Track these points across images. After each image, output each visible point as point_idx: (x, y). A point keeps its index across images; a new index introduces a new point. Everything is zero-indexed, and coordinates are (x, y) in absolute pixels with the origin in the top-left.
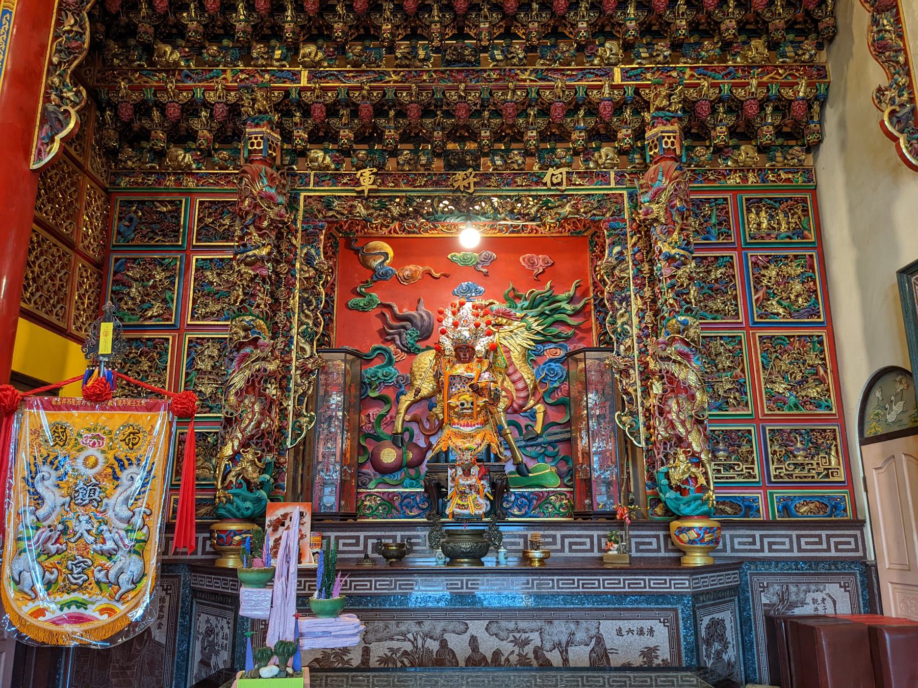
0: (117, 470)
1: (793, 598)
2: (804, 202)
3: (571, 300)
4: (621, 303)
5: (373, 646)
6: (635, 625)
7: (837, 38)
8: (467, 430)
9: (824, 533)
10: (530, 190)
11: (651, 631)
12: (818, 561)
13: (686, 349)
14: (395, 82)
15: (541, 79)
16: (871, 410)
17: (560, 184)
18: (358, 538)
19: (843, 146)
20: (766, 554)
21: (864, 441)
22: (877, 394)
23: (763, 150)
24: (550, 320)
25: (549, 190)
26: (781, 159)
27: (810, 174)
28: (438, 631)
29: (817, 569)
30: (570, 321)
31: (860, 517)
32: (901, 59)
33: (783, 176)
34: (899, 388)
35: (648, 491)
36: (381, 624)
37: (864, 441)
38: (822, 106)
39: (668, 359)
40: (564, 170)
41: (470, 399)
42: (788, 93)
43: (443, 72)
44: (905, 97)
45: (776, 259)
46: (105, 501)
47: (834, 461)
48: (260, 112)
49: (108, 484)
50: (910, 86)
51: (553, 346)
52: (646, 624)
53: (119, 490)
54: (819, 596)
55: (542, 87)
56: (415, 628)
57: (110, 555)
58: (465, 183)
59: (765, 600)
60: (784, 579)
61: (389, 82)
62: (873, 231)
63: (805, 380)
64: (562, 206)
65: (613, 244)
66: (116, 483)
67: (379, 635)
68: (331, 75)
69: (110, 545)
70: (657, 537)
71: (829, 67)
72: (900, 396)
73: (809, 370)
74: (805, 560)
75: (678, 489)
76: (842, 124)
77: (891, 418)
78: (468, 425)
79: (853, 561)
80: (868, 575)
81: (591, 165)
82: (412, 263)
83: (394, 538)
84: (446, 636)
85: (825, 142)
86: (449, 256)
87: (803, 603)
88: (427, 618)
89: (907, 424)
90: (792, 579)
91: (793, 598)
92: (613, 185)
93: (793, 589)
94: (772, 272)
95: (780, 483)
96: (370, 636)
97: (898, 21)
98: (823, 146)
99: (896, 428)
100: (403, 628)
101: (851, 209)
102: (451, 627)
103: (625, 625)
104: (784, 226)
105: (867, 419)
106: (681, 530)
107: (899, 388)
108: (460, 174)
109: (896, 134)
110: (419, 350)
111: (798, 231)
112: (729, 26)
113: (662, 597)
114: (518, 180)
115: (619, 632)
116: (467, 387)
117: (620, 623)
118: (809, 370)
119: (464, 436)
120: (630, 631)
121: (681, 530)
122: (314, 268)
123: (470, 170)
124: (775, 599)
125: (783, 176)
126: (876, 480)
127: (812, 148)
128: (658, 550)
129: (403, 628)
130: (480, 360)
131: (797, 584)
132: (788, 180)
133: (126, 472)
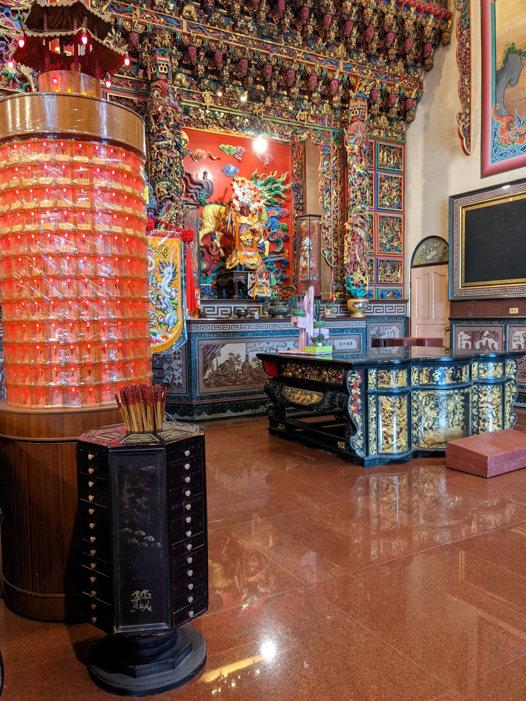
0: (161, 268)
1: (381, 332)
2: (399, 151)
3: (284, 183)
4: (326, 193)
5: (249, 354)
6: (346, 341)
7: (432, 71)
8: (250, 254)
9: (394, 305)
10: (289, 121)
11: (351, 343)
12: (390, 317)
13: (363, 221)
14: (234, 42)
15: (308, 59)
16: (418, 253)
17: (304, 121)
18: (214, 308)
19: (426, 128)
20: (375, 314)
21: (413, 267)
22: (423, 246)
23: (390, 119)
24: (273, 193)
25: (298, 123)
26: (395, 126)
27: (404, 135)
28: (275, 346)
29: (391, 319)
30: (283, 196)
31: (405, 299)
32: (468, 100)
33: (394, 135)
34: (436, 245)
35: (334, 287)
36: (253, 344)
37: (413, 267)
38: (417, 103)
39: (357, 226)
40: (306, 113)
41: (251, 237)
42: (407, 94)
43: (260, 42)
44: (467, 120)
45: (388, 178)
46: (159, 284)
47: (399, 274)
48: (165, 46)
49: (159, 276)
50: (469, 114)
51: (274, 209)
52: (350, 341)
53: (165, 279)
54: (389, 331)
55: (307, 64)
56: (266, 345)
57: (163, 310)
58: (259, 111)
59: (372, 333)
60: (379, 324)
61: (231, 41)
62: (435, 175)
63: (393, 238)
64: (302, 134)
65: (325, 159)
66: (161, 275)
67: (252, 349)
68: (200, 28)
69: (164, 306)
70: (337, 307)
71: (424, 84)
72: (436, 248)
73: (395, 234)
74: (386, 316)
75: (356, 285)
76: (427, 116)
77: (429, 257)
78: (250, 251)
79: (402, 317)
80: (407, 321)
81: (317, 112)
82: (203, 149)
83: (244, 307)
84: (278, 348)
85: (415, 121)
86: (220, 147)
87: (384, 334)
88: (271, 341)
89: (437, 260)
90: (382, 324)
91: (381, 332)
92: (326, 126)
93: (381, 328)
94: (386, 185)
95: (382, 284)
96: (249, 350)
97: (469, 81)
98: (413, 124)
99: (431, 262)
100: (262, 346)
101: (425, 160)
102: (280, 344)
103: (343, 341)
104: (392, 162)
105: (415, 257)
106: (355, 303)
107: (436, 245)
108: (257, 105)
109: (463, 136)
110: (206, 204)
111: (397, 165)
112: (393, 51)
113: (357, 330)
114: (284, 114)
115: (341, 344)
116: (249, 231)
117: (341, 341)
118: (395, 234)
119: (249, 257)
120: (344, 344)
121: (355, 303)
122: (180, 152)
123: (261, 104)
124: (375, 333)
125: (394, 135)
126: (416, 283)
127: (409, 123)
128: (337, 313)
129: (262, 346)
130: (253, 215)
131: (383, 326)
132: (396, 137)
133: (166, 269)
